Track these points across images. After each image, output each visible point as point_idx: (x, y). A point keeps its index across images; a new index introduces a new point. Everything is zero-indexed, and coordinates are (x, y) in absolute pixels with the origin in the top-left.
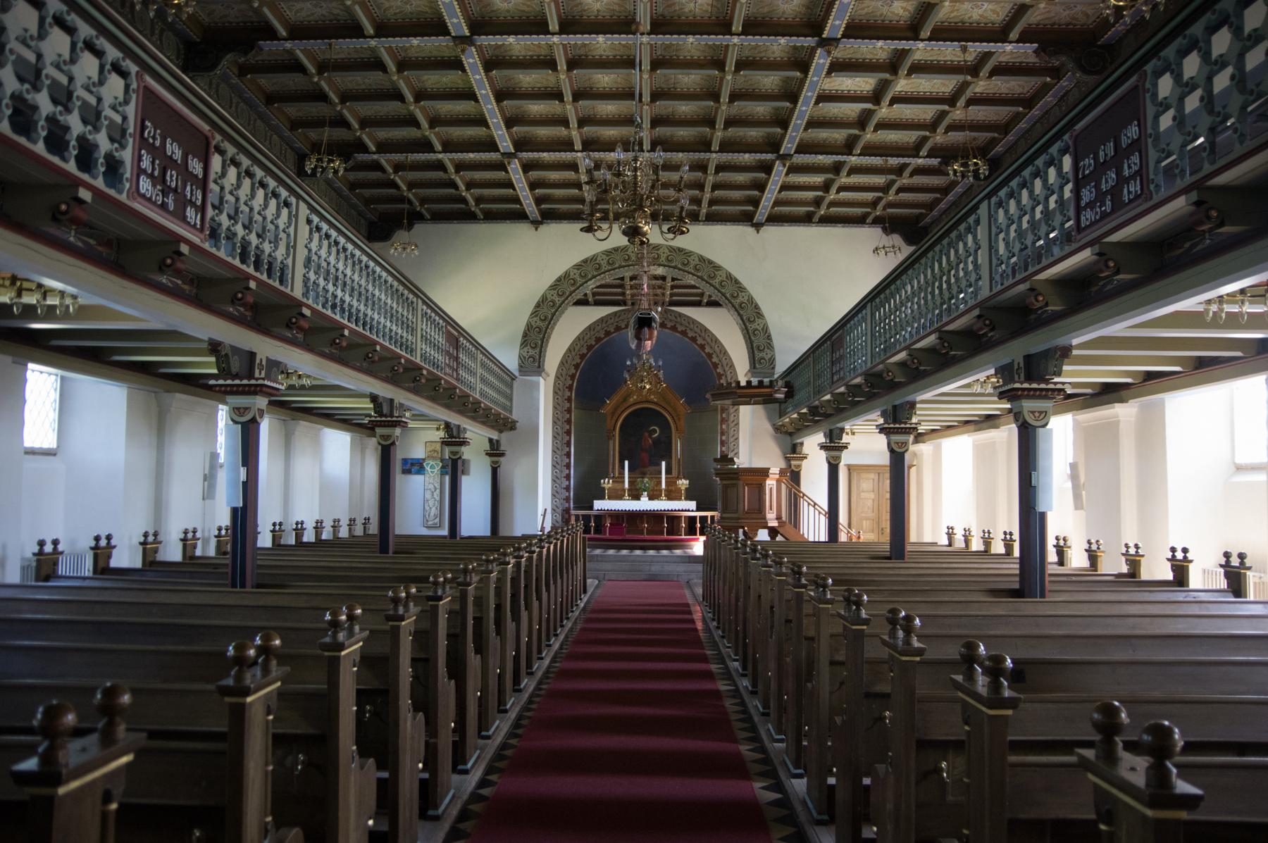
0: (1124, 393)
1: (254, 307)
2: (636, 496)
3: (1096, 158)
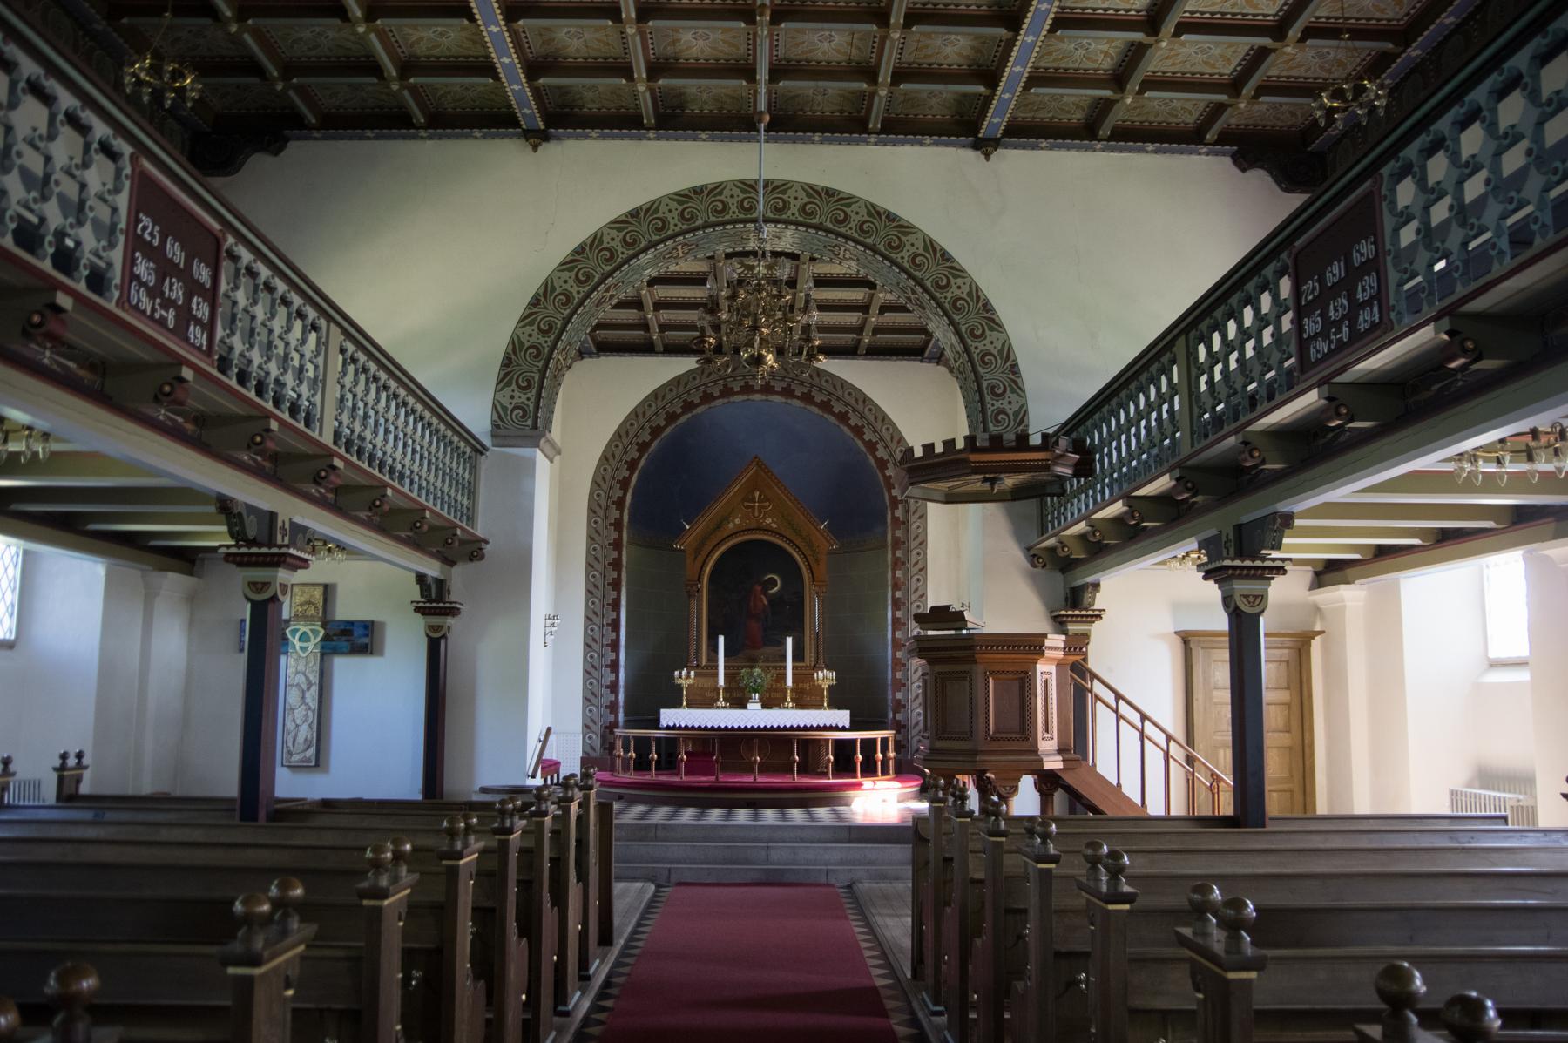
0: (1350, 572)
1: (275, 458)
2: (740, 703)
3: (1322, 281)
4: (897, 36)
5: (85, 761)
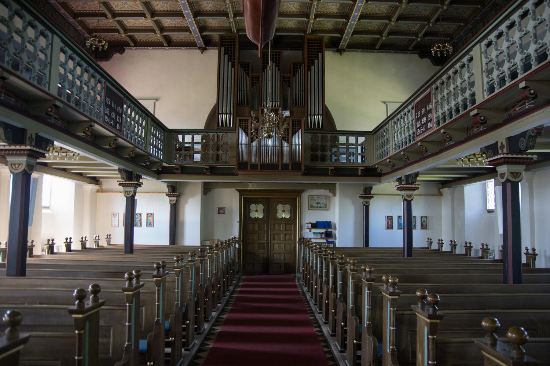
4: (312, 21)
5: (87, 239)
